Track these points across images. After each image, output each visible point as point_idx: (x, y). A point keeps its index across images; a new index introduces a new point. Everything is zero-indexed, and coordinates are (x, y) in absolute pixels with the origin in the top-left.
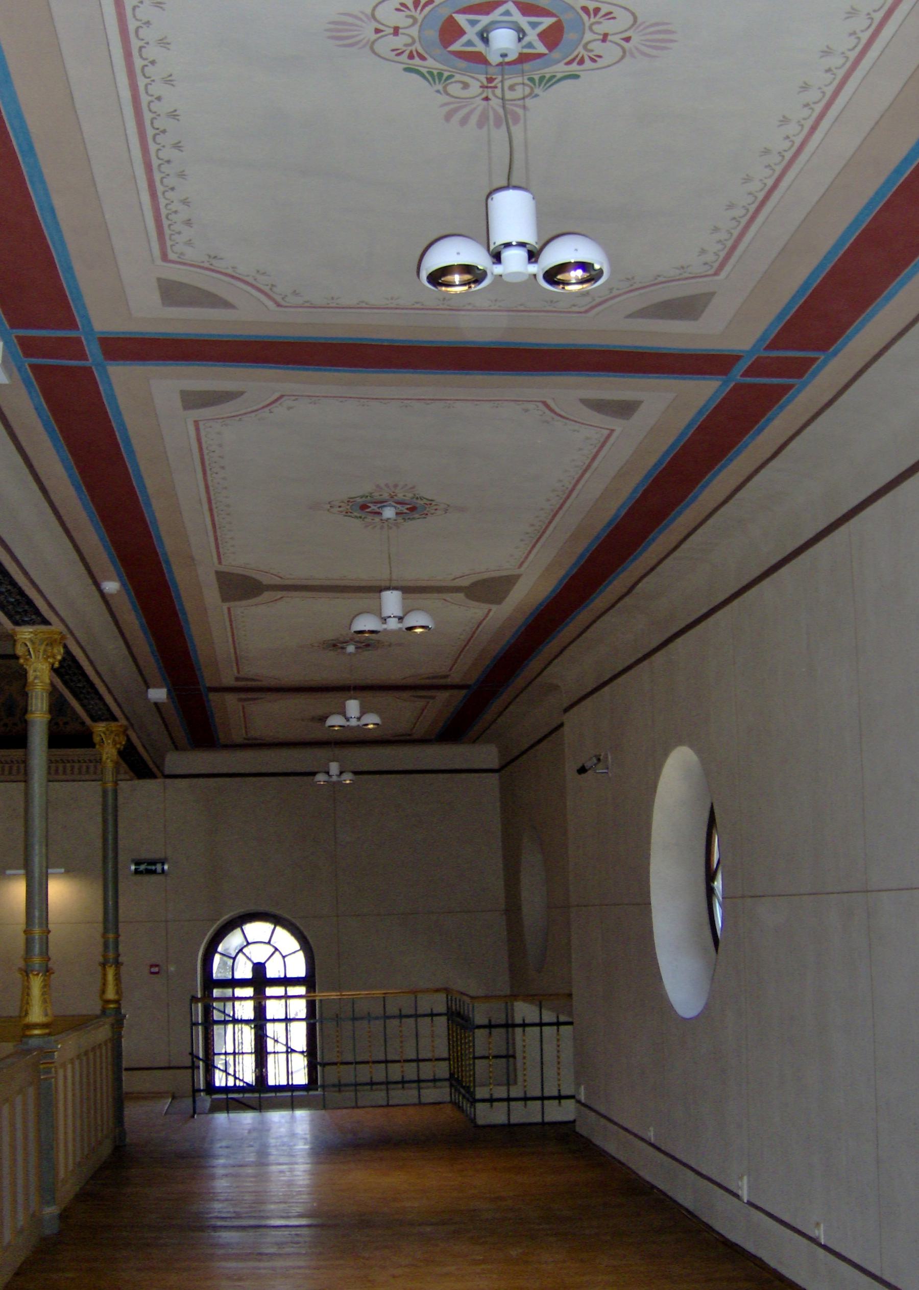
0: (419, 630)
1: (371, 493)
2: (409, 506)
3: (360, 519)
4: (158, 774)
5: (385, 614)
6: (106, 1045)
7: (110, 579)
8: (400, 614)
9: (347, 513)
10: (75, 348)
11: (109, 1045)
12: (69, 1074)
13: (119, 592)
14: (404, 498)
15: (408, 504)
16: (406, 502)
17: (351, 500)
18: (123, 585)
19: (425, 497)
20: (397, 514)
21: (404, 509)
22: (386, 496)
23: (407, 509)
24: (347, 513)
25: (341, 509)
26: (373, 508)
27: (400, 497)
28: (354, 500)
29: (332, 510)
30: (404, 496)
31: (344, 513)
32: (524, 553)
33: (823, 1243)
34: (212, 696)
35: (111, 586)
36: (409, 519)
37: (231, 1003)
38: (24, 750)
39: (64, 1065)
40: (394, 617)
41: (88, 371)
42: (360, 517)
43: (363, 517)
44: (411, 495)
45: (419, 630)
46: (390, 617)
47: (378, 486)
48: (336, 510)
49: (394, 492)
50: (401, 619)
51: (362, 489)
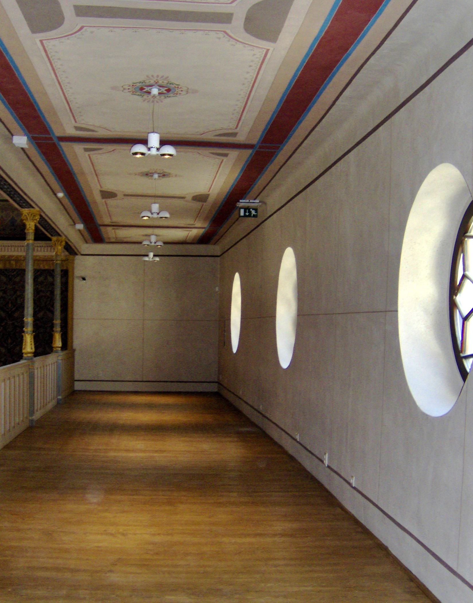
0: (159, 247)
1: (144, 81)
2: (166, 89)
3: (140, 96)
4: (79, 254)
5: (153, 211)
6: (23, 374)
7: (60, 192)
8: (158, 212)
9: (133, 92)
10: (51, 139)
11: (25, 375)
12: (17, 383)
13: (63, 197)
14: (163, 83)
15: (166, 87)
16: (164, 86)
17: (135, 85)
18: (65, 195)
19: (175, 83)
20: (159, 93)
21: (163, 90)
22: (152, 82)
23: (166, 90)
24: (133, 92)
25: (129, 90)
26: (147, 89)
27: (160, 82)
28: (136, 84)
29: (125, 91)
30: (163, 82)
31: (132, 92)
32: (246, 96)
33: (353, 486)
34: (62, 144)
35: (61, 195)
36: (167, 96)
37: (76, 383)
38: (33, 239)
39: (37, 368)
40: (156, 213)
41: (54, 144)
42: (141, 95)
43: (142, 95)
44: (166, 82)
45: (159, 247)
46: (154, 213)
47: (147, 76)
48: (127, 91)
49: (157, 80)
50: (158, 214)
51: (138, 78)
